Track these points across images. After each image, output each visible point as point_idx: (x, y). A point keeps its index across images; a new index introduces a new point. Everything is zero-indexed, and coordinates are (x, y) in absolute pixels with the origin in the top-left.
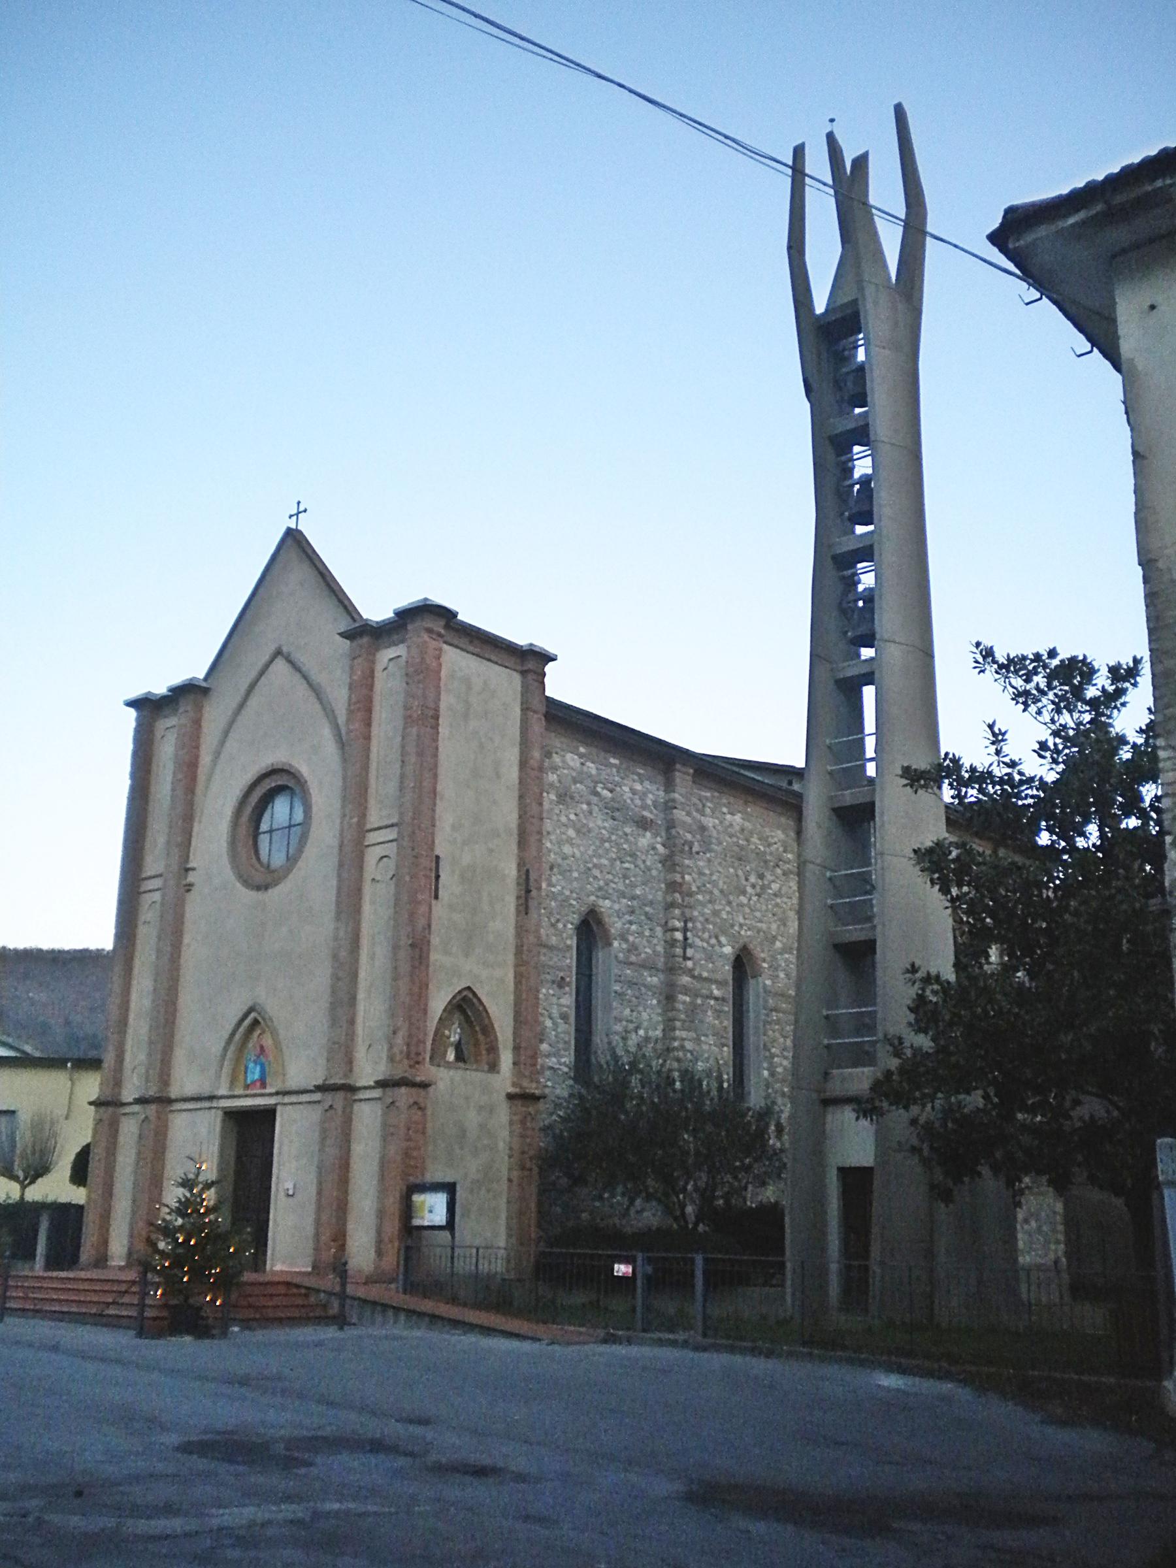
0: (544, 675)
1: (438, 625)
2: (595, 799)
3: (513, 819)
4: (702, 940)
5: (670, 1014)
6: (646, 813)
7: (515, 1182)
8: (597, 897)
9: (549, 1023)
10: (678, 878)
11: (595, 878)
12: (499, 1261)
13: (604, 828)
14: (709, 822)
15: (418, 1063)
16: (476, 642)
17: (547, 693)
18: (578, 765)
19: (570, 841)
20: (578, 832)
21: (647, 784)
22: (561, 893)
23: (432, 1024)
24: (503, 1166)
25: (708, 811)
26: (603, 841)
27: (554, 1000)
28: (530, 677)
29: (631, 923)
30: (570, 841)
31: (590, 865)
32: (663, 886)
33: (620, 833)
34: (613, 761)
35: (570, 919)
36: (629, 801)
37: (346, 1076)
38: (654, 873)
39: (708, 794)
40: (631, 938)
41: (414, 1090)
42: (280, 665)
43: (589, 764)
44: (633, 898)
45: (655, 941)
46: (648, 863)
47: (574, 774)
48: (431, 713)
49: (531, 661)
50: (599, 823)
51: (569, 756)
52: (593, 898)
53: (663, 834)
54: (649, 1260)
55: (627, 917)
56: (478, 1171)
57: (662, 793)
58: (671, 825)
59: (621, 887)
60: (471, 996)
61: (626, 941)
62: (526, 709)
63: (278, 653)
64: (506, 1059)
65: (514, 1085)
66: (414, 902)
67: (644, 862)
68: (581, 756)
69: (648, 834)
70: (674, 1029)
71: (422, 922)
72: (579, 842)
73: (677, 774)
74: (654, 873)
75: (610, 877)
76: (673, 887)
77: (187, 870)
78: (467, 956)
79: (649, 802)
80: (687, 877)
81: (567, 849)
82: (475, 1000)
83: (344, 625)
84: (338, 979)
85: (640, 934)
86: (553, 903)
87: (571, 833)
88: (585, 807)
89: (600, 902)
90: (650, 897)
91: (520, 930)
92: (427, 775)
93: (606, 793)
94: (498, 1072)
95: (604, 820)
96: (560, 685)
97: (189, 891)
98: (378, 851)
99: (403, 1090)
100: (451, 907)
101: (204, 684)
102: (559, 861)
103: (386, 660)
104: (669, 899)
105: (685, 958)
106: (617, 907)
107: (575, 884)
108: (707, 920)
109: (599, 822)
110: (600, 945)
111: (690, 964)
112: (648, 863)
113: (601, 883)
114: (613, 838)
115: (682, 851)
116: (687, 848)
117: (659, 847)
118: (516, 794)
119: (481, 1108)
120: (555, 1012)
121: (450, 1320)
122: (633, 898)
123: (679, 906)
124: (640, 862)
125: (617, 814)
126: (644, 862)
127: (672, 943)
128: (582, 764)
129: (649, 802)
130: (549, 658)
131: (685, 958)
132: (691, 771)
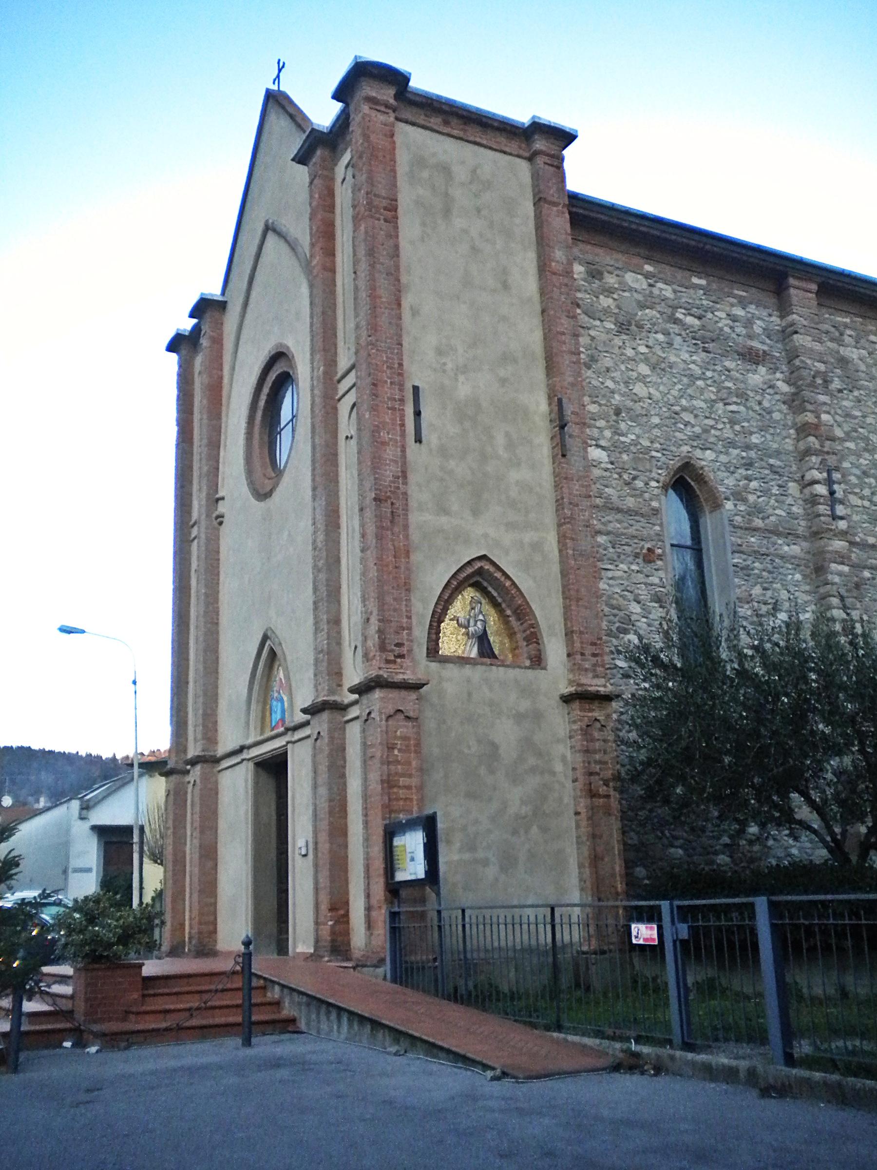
0: (563, 159)
1: (388, 94)
2: (676, 328)
3: (535, 339)
4: (862, 498)
5: (822, 590)
6: (755, 344)
7: (584, 815)
8: (692, 447)
9: (635, 608)
10: (810, 418)
11: (687, 424)
12: (575, 928)
13: (694, 362)
14: (853, 354)
15: (402, 656)
16: (454, 121)
17: (572, 185)
18: (645, 286)
19: (642, 379)
20: (653, 368)
21: (752, 308)
22: (635, 443)
23: (423, 608)
24: (567, 794)
25: (847, 339)
26: (693, 378)
27: (640, 577)
28: (540, 160)
29: (749, 479)
30: (642, 379)
31: (677, 408)
32: (792, 431)
33: (719, 368)
34: (695, 280)
35: (654, 475)
36: (727, 329)
37: (331, 692)
38: (776, 416)
39: (848, 320)
40: (752, 498)
41: (394, 694)
42: (271, 238)
43: (660, 285)
44: (748, 447)
45: (789, 500)
46: (766, 404)
47: (640, 298)
48: (384, 203)
49: (546, 142)
50: (686, 356)
51: (629, 277)
52: (685, 448)
53: (784, 368)
54: (684, 914)
55: (742, 471)
56: (523, 802)
57: (775, 319)
58: (792, 355)
59: (728, 433)
60: (487, 567)
61: (744, 500)
62: (539, 201)
63: (268, 228)
64: (555, 650)
65: (571, 682)
66: (379, 444)
67: (760, 403)
68: (647, 276)
69: (762, 370)
70: (830, 607)
71: (389, 472)
72: (654, 379)
73: (792, 291)
74: (776, 416)
75: (711, 422)
76: (804, 430)
77: (218, 500)
78: (476, 512)
79: (759, 331)
80: (824, 417)
81: (639, 389)
82: (498, 575)
83: (296, 142)
84: (319, 571)
85: (766, 492)
86: (625, 457)
87: (644, 369)
88: (660, 337)
89: (698, 453)
90: (775, 446)
91: (560, 479)
92: (383, 282)
93: (689, 320)
94: (545, 668)
95: (692, 354)
96: (587, 173)
97: (221, 523)
98: (351, 398)
99: (377, 694)
100: (443, 452)
101: (221, 299)
102: (630, 404)
103: (343, 169)
104: (802, 446)
105: (835, 517)
106: (723, 458)
107: (656, 432)
108: (864, 473)
109: (682, 355)
110: (707, 509)
111: (842, 525)
112: (766, 404)
113: (698, 430)
114: (709, 374)
115: (812, 385)
116: (819, 381)
117: (779, 384)
118: (538, 308)
119: (519, 718)
120: (643, 593)
121: (391, 1029)
122: (748, 447)
123: (817, 453)
124: (752, 403)
125: (710, 346)
126: (760, 403)
127: (813, 500)
128: (650, 285)
129: (759, 331)
130: (567, 137)
131: (835, 517)
132: (814, 287)
